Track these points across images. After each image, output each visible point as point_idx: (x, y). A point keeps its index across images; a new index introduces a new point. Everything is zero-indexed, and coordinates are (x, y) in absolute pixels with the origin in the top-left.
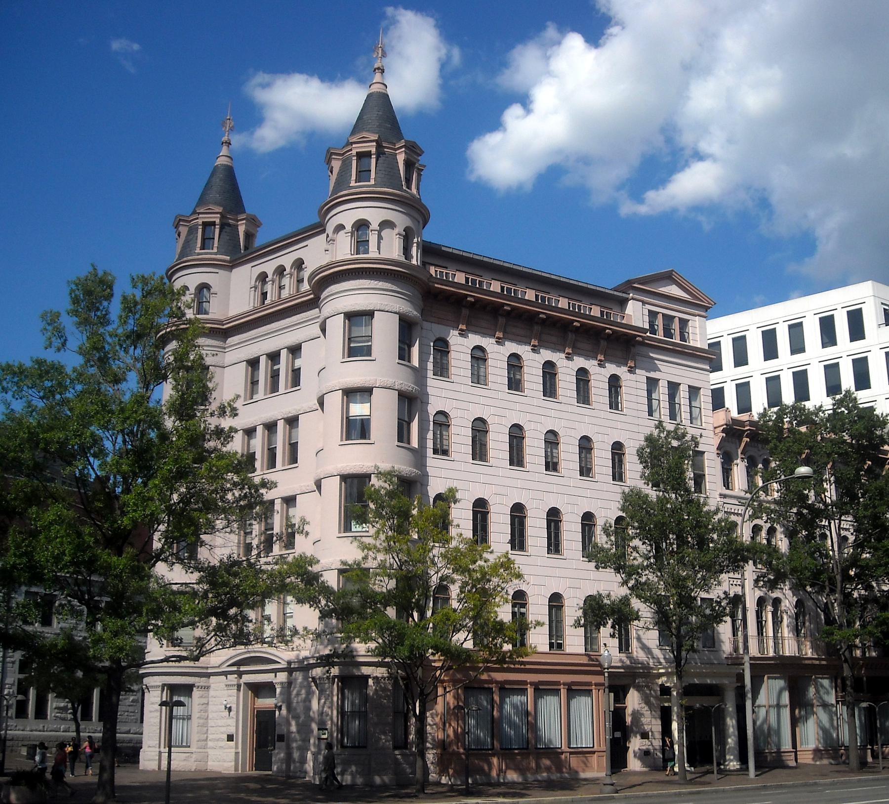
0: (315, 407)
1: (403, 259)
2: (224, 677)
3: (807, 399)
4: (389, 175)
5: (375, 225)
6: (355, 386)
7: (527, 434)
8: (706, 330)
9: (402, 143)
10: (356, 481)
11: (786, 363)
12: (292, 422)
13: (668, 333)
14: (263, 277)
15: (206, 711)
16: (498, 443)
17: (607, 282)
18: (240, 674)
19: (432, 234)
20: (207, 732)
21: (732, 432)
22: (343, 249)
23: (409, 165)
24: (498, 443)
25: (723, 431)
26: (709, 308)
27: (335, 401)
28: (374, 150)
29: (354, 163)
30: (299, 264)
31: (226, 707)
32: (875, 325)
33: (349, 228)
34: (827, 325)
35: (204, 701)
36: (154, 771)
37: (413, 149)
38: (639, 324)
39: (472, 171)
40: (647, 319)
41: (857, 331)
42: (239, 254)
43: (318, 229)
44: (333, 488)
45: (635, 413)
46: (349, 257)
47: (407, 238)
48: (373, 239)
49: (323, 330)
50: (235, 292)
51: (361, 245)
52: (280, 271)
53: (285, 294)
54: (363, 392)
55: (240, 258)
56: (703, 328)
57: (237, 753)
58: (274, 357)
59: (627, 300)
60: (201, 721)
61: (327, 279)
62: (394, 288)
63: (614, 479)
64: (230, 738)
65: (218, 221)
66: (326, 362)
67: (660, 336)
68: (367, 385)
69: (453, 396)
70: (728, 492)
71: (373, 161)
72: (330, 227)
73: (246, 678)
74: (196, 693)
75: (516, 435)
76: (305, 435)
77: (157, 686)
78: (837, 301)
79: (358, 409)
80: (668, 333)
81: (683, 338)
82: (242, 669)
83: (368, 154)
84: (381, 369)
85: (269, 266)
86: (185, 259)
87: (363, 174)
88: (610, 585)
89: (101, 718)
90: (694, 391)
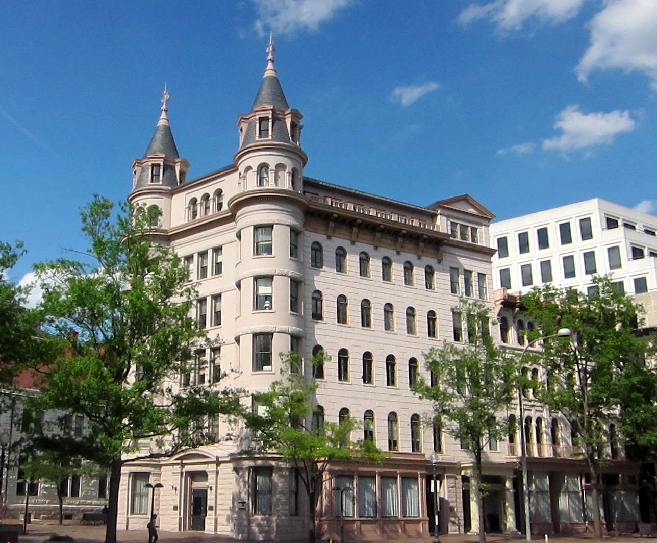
0: (232, 288)
1: (291, 189)
2: (171, 467)
4: (280, 132)
5: (272, 167)
7: (349, 302)
9: (289, 111)
10: (262, 337)
12: (217, 297)
13: (463, 236)
14: (194, 201)
16: (354, 312)
17: (422, 202)
18: (183, 465)
19: (308, 172)
21: (509, 303)
22: (251, 184)
23: (293, 125)
24: (354, 312)
25: (502, 304)
27: (248, 285)
28: (270, 116)
29: (258, 125)
30: (219, 193)
31: (173, 488)
32: (600, 229)
33: (255, 169)
34: (565, 230)
37: (296, 115)
38: (445, 231)
39: (560, 120)
40: (450, 228)
41: (587, 234)
42: (176, 187)
43: (233, 168)
44: (247, 343)
45: (442, 291)
47: (294, 174)
49: (239, 236)
50: (176, 212)
52: (206, 197)
53: (210, 213)
54: (269, 278)
55: (178, 188)
57: (180, 519)
58: (203, 254)
61: (240, 204)
62: (277, 207)
63: (429, 336)
64: (175, 508)
65: (162, 163)
66: (240, 259)
67: (458, 238)
68: (270, 274)
69: (328, 282)
70: (505, 345)
71: (270, 124)
72: (242, 169)
73: (187, 468)
75: (366, 306)
76: (225, 306)
78: (572, 213)
79: (263, 290)
80: (463, 236)
81: (473, 240)
82: (184, 461)
83: (267, 119)
84: (279, 262)
85: (198, 193)
86: (140, 189)
87: (263, 132)
88: (426, 408)
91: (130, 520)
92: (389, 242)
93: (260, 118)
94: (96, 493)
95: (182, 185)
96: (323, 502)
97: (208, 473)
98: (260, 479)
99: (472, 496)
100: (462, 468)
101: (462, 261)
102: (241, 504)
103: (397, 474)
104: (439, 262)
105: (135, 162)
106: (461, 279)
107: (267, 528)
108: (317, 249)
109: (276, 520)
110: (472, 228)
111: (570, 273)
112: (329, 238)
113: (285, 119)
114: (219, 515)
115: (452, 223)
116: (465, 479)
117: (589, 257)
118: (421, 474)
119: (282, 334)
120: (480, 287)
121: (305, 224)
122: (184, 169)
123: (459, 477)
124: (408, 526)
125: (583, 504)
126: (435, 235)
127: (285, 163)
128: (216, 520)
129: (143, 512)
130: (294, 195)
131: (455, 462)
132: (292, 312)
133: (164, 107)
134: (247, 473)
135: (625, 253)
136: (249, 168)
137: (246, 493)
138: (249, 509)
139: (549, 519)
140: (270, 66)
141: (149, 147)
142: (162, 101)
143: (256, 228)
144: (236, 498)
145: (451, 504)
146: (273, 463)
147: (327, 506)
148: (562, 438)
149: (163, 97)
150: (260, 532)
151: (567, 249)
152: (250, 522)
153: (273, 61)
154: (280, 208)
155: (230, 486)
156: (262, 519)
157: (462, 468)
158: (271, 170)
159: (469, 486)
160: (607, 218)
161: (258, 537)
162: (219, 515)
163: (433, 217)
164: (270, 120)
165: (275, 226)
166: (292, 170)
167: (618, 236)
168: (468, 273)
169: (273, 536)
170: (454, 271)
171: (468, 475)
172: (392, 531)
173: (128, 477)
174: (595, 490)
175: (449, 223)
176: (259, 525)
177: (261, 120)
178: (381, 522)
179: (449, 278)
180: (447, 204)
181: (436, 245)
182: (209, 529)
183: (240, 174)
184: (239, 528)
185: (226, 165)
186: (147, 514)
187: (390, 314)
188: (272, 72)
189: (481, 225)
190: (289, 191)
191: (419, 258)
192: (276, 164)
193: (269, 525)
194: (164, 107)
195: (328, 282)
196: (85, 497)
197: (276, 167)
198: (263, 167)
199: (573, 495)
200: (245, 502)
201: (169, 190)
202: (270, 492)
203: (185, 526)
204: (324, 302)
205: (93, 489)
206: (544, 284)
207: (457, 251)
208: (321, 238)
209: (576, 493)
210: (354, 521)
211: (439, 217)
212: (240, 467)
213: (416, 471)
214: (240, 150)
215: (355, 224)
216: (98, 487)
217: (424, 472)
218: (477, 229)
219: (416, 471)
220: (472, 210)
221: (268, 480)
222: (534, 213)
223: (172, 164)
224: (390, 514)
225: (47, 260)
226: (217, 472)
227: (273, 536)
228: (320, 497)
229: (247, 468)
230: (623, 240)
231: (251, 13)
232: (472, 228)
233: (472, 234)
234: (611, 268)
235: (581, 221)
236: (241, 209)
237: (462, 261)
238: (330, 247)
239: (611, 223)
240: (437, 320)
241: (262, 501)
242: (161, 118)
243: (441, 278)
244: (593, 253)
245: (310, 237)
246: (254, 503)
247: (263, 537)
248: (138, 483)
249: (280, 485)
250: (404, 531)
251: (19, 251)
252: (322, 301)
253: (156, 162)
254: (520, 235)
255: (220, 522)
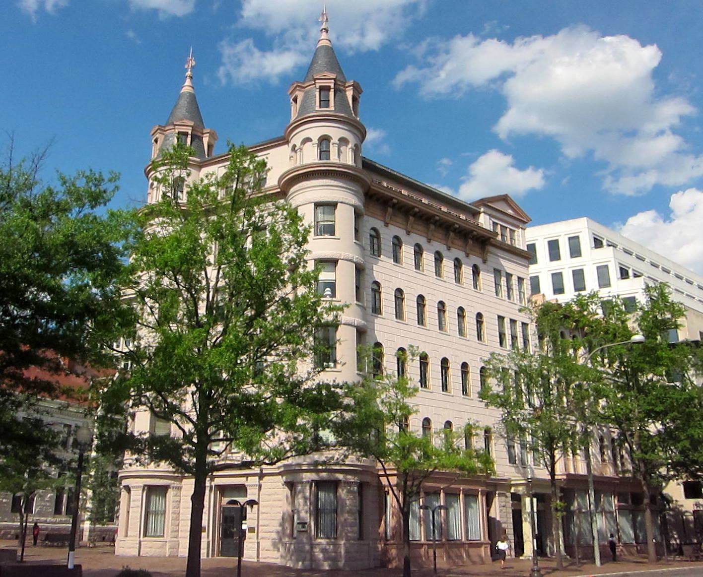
1: (354, 165)
3: (584, 289)
5: (335, 140)
6: (326, 257)
8: (523, 238)
11: (566, 264)
15: (179, 507)
19: (369, 153)
20: (178, 525)
22: (310, 156)
23: (355, 99)
26: (526, 223)
33: (315, 141)
35: (177, 499)
36: (134, 557)
37: (357, 89)
41: (575, 252)
46: (317, 161)
48: (333, 150)
51: (324, 153)
56: (523, 236)
59: (479, 213)
60: (174, 516)
62: (341, 184)
65: (190, 132)
69: (384, 271)
72: (296, 140)
74: (170, 493)
77: (138, 487)
87: (324, 102)
88: (493, 417)
89: (68, 512)
90: (520, 280)
91: (142, 543)
92: (440, 236)
93: (320, 86)
94: (52, 510)
95: (210, 158)
96: (391, 520)
97: (248, 488)
98: (321, 495)
99: (525, 516)
100: (511, 486)
101: (503, 262)
102: (301, 526)
103: (460, 490)
104: (485, 261)
105: (157, 128)
106: (503, 281)
107: (333, 554)
108: (376, 235)
109: (345, 544)
110: (510, 229)
111: (559, 290)
112: (386, 225)
113: (345, 91)
114: (262, 538)
115: (494, 223)
116: (516, 498)
117: (578, 275)
118: (482, 491)
119: (349, 327)
120: (520, 292)
121: (366, 205)
122: (212, 142)
123: (509, 495)
124: (472, 551)
125: (617, 525)
126: (482, 232)
127: (347, 137)
128: (258, 543)
129: (158, 534)
130: (355, 171)
131: (505, 478)
132: (358, 303)
133: (189, 73)
134: (308, 488)
135: (614, 273)
136: (308, 140)
137: (306, 512)
138: (311, 531)
139: (384, 535)
140: (188, 82)
141: (172, 114)
142: (186, 67)
143: (317, 205)
144: (289, 518)
145: (503, 525)
146: (340, 476)
147: (394, 528)
148: (593, 454)
149: (187, 62)
150: (325, 559)
151: (556, 266)
152: (312, 546)
153: (191, 78)
154: (345, 186)
155: (280, 503)
156: (328, 544)
157: (511, 486)
158: (333, 144)
159: (520, 505)
160: (595, 238)
161: (323, 565)
162: (262, 538)
163: (476, 214)
164: (189, 136)
165: (339, 204)
166: (355, 145)
167: (606, 255)
168: (509, 276)
169: (341, 564)
170: (497, 272)
171: (521, 493)
172: (457, 556)
173: (141, 492)
174: (648, 510)
175: (491, 222)
176: (324, 551)
177: (322, 89)
178: (447, 546)
179: (493, 279)
180: (491, 202)
181: (481, 243)
182: (249, 554)
183: (295, 146)
184: (299, 553)
185: (275, 137)
186: (163, 536)
187: (442, 313)
188: (191, 88)
189: (518, 227)
190: (352, 166)
191: (467, 255)
192: (339, 137)
193: (336, 551)
194: (189, 73)
195: (384, 271)
196: (40, 514)
197: (339, 140)
198: (323, 140)
199: (609, 515)
200: (306, 523)
201: (197, 162)
202: (336, 511)
203: (213, 550)
204: (383, 295)
205: (48, 504)
206: (577, 293)
207: (500, 253)
208: (378, 224)
209: (611, 513)
210: (422, 545)
211: (482, 215)
212: (298, 480)
213: (476, 488)
214: (292, 121)
215: (411, 212)
216: (54, 503)
217: (484, 488)
218: (514, 231)
219: (476, 488)
220: (510, 212)
221: (332, 495)
222: (539, 225)
223: (199, 134)
224: (453, 536)
225: (127, 207)
226: (260, 487)
227: (341, 564)
228: (384, 517)
229: (308, 482)
230: (613, 260)
231: (240, 6)
232: (510, 229)
233: (511, 235)
234: (600, 286)
235: (570, 239)
236: (300, 182)
237: (503, 262)
238: (388, 233)
239: (598, 243)
240: (485, 323)
241: (326, 520)
242: (186, 84)
243: (486, 278)
244: (582, 270)
245: (371, 222)
246: (316, 524)
247: (330, 566)
248: (153, 498)
249: (348, 502)
250: (468, 556)
251: (110, 187)
252: (380, 293)
253: (183, 129)
254: (549, 242)
255: (262, 545)
